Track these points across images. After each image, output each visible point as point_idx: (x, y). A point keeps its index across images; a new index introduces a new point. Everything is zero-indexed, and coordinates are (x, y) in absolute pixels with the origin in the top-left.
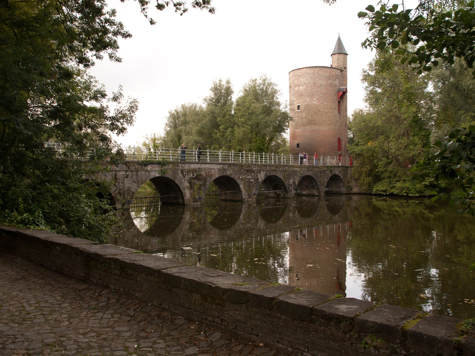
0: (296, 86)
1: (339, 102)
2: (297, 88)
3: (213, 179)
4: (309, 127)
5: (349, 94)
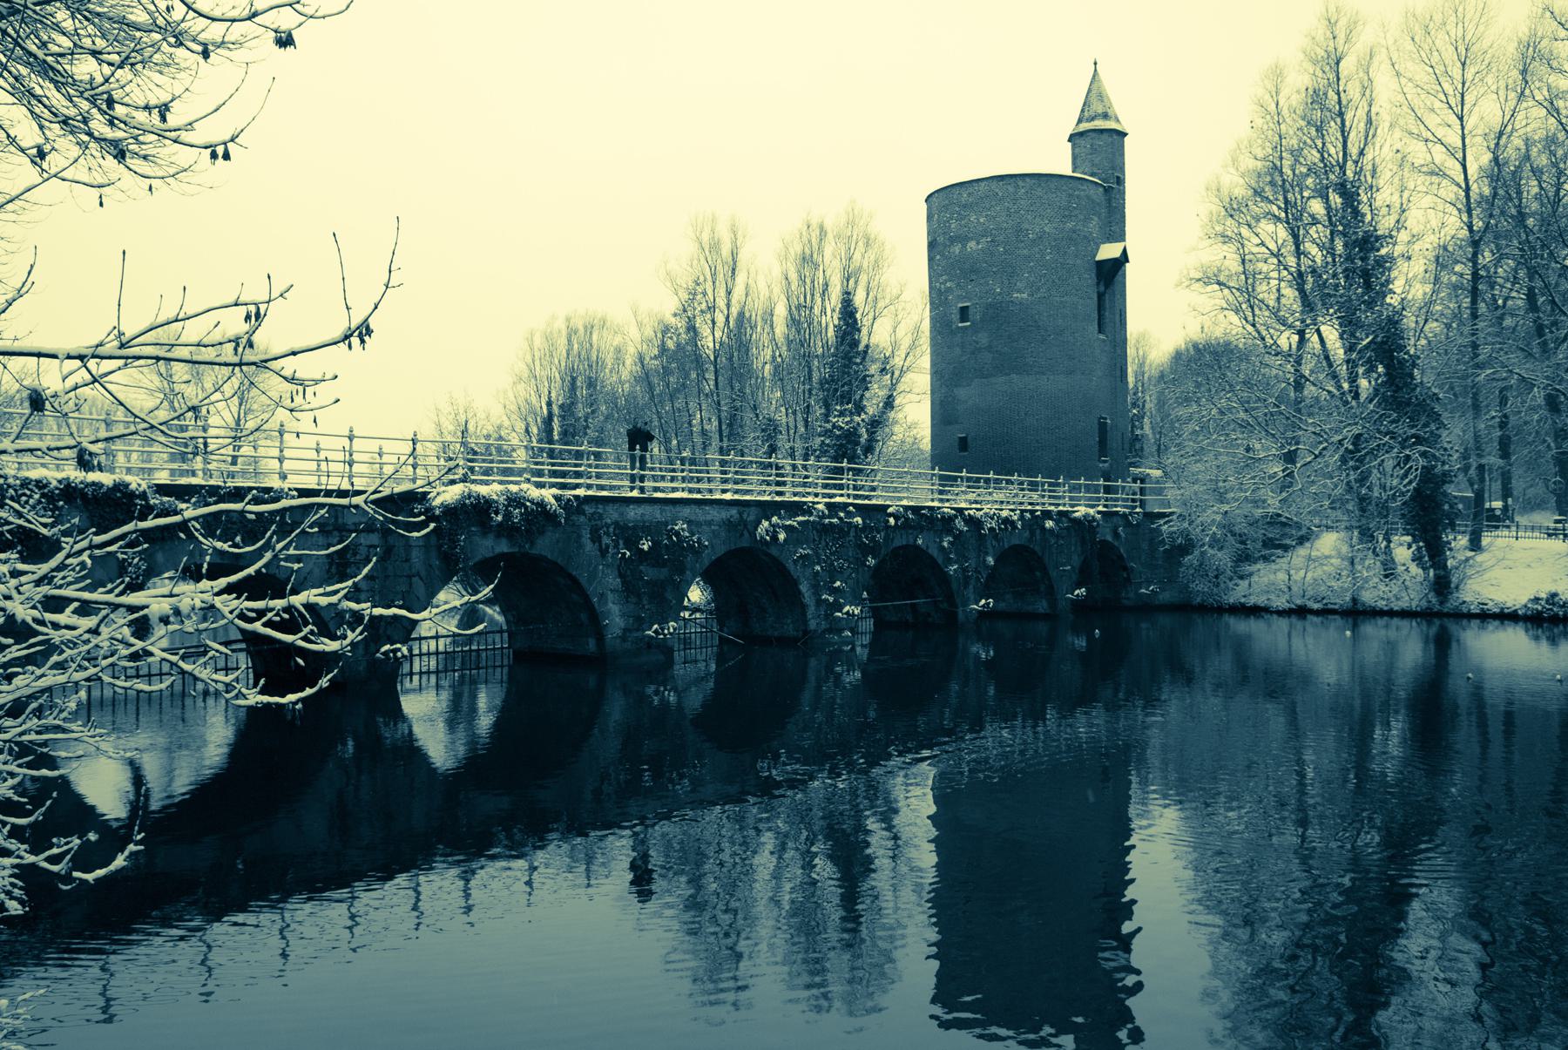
0: (952, 240)
1: (1100, 296)
2: (957, 249)
3: (706, 563)
4: (1002, 379)
5: (1133, 274)
